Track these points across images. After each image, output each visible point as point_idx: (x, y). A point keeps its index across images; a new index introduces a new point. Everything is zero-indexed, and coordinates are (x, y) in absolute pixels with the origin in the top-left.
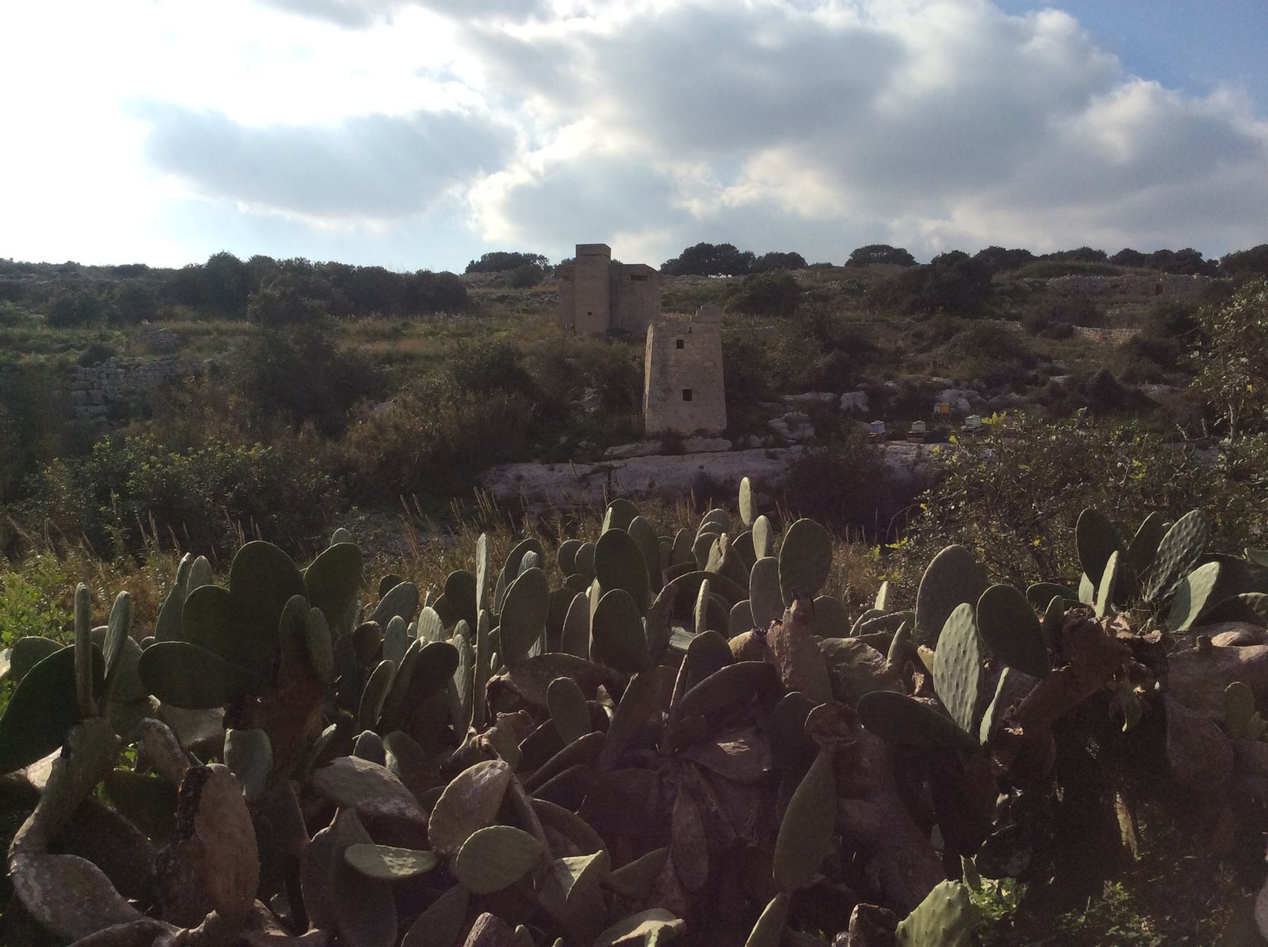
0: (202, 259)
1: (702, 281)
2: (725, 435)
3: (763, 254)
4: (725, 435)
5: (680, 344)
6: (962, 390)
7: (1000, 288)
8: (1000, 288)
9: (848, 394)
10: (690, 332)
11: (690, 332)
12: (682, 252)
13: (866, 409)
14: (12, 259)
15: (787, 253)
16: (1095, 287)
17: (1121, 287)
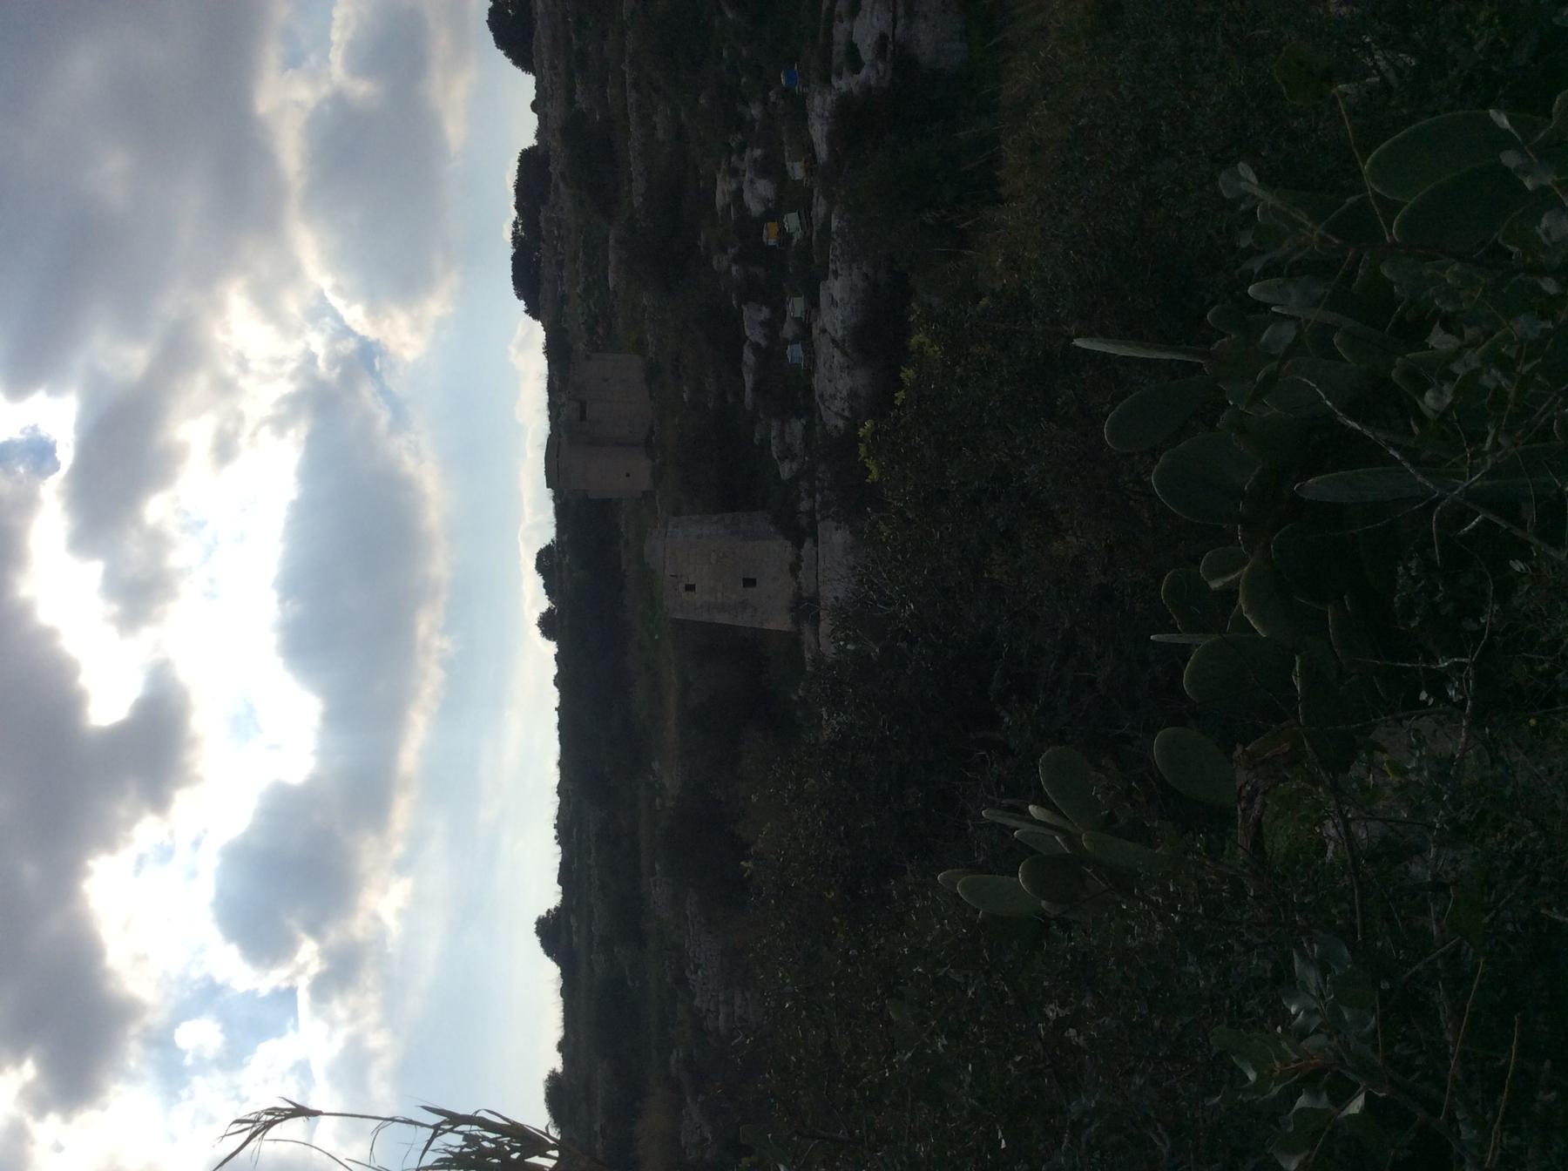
0: (511, 262)
2: (798, 544)
3: (533, 120)
4: (798, 544)
5: (690, 588)
7: (554, 78)
8: (554, 78)
10: (676, 576)
11: (676, 576)
12: (501, 53)
14: (556, 709)
15: (557, 671)
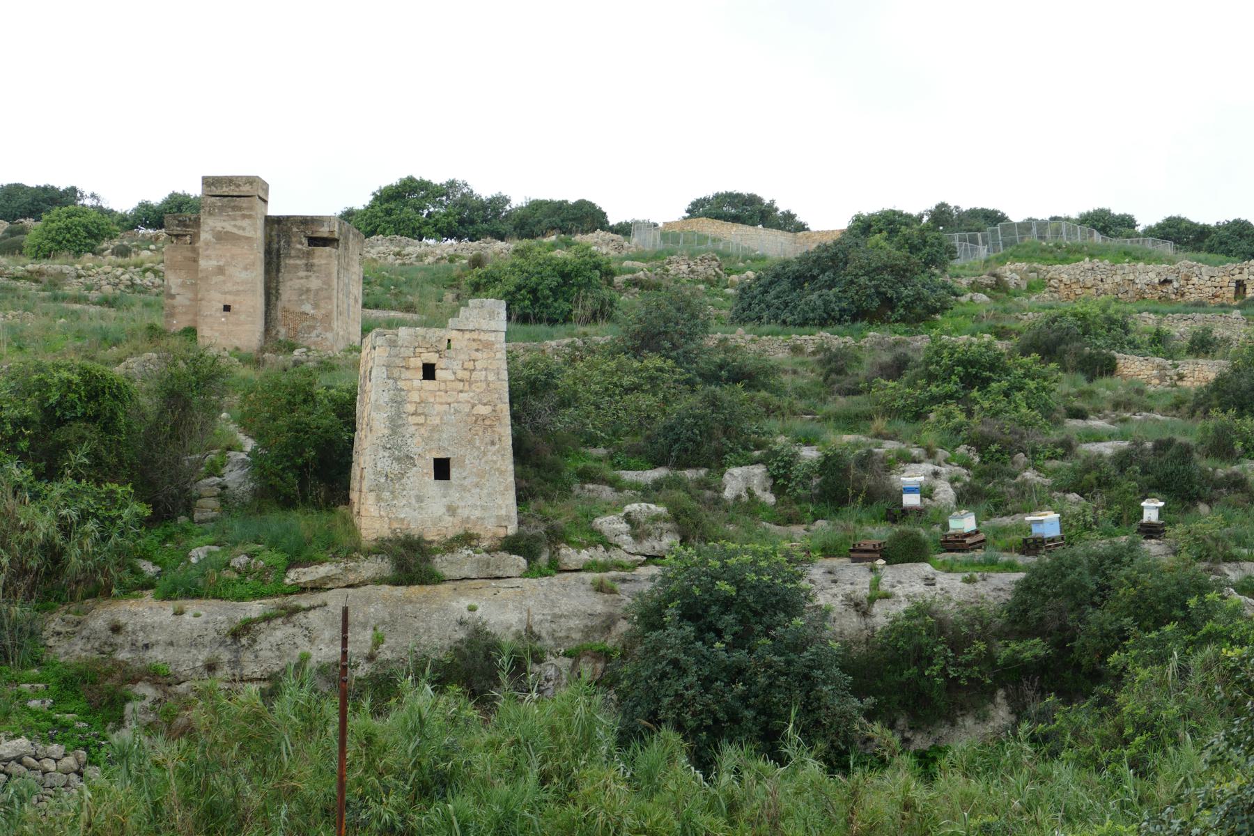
1: (414, 248)
6: (939, 465)
9: (736, 471)
13: (770, 498)
16: (1133, 281)
17: (1176, 284)
